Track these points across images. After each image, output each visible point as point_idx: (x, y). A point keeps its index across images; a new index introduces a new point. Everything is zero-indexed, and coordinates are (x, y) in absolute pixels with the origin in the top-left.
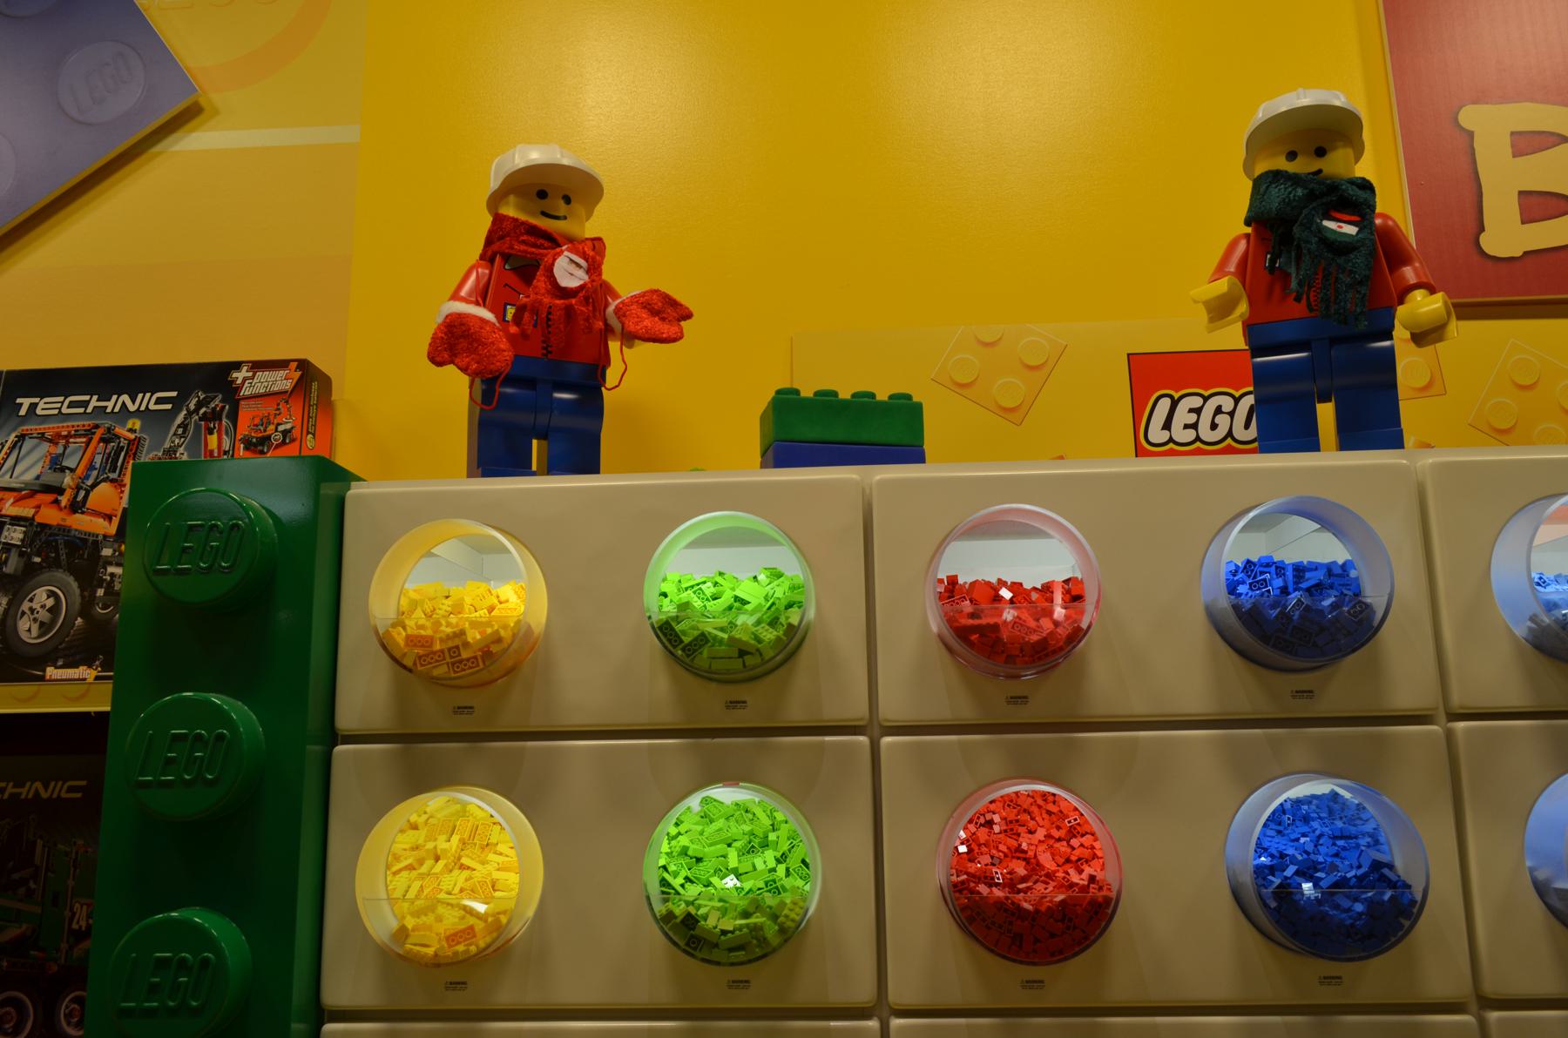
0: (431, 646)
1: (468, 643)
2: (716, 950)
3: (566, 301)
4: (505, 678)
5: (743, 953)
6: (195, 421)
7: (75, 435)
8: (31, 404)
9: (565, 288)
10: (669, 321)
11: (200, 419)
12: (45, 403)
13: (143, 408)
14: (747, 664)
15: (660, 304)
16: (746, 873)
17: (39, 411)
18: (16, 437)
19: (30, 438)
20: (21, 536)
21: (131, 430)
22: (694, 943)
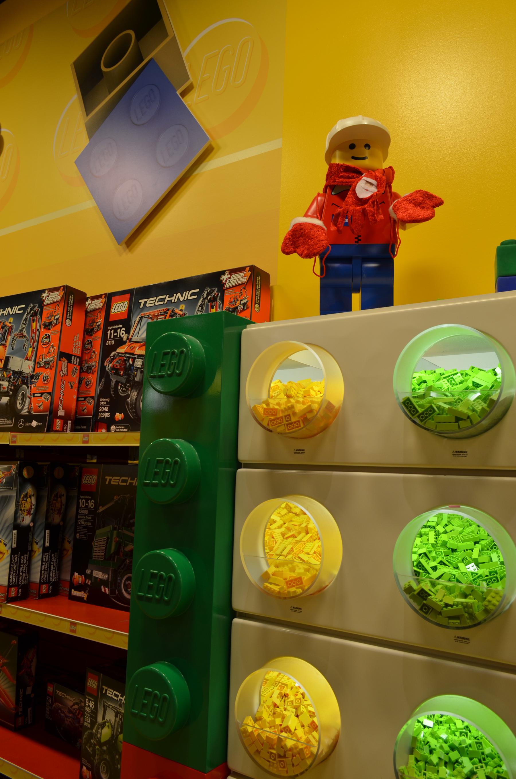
0: (276, 415)
1: (296, 413)
2: (440, 616)
3: (363, 207)
4: (321, 434)
5: (459, 621)
6: (206, 303)
7: (160, 315)
8: (145, 302)
9: (362, 199)
10: (427, 208)
11: (209, 302)
12: (150, 301)
13: (185, 299)
14: (461, 427)
15: (421, 199)
16: (484, 563)
17: (147, 305)
18: (139, 318)
19: (144, 318)
20: (141, 364)
21: (181, 310)
22: (425, 609)
